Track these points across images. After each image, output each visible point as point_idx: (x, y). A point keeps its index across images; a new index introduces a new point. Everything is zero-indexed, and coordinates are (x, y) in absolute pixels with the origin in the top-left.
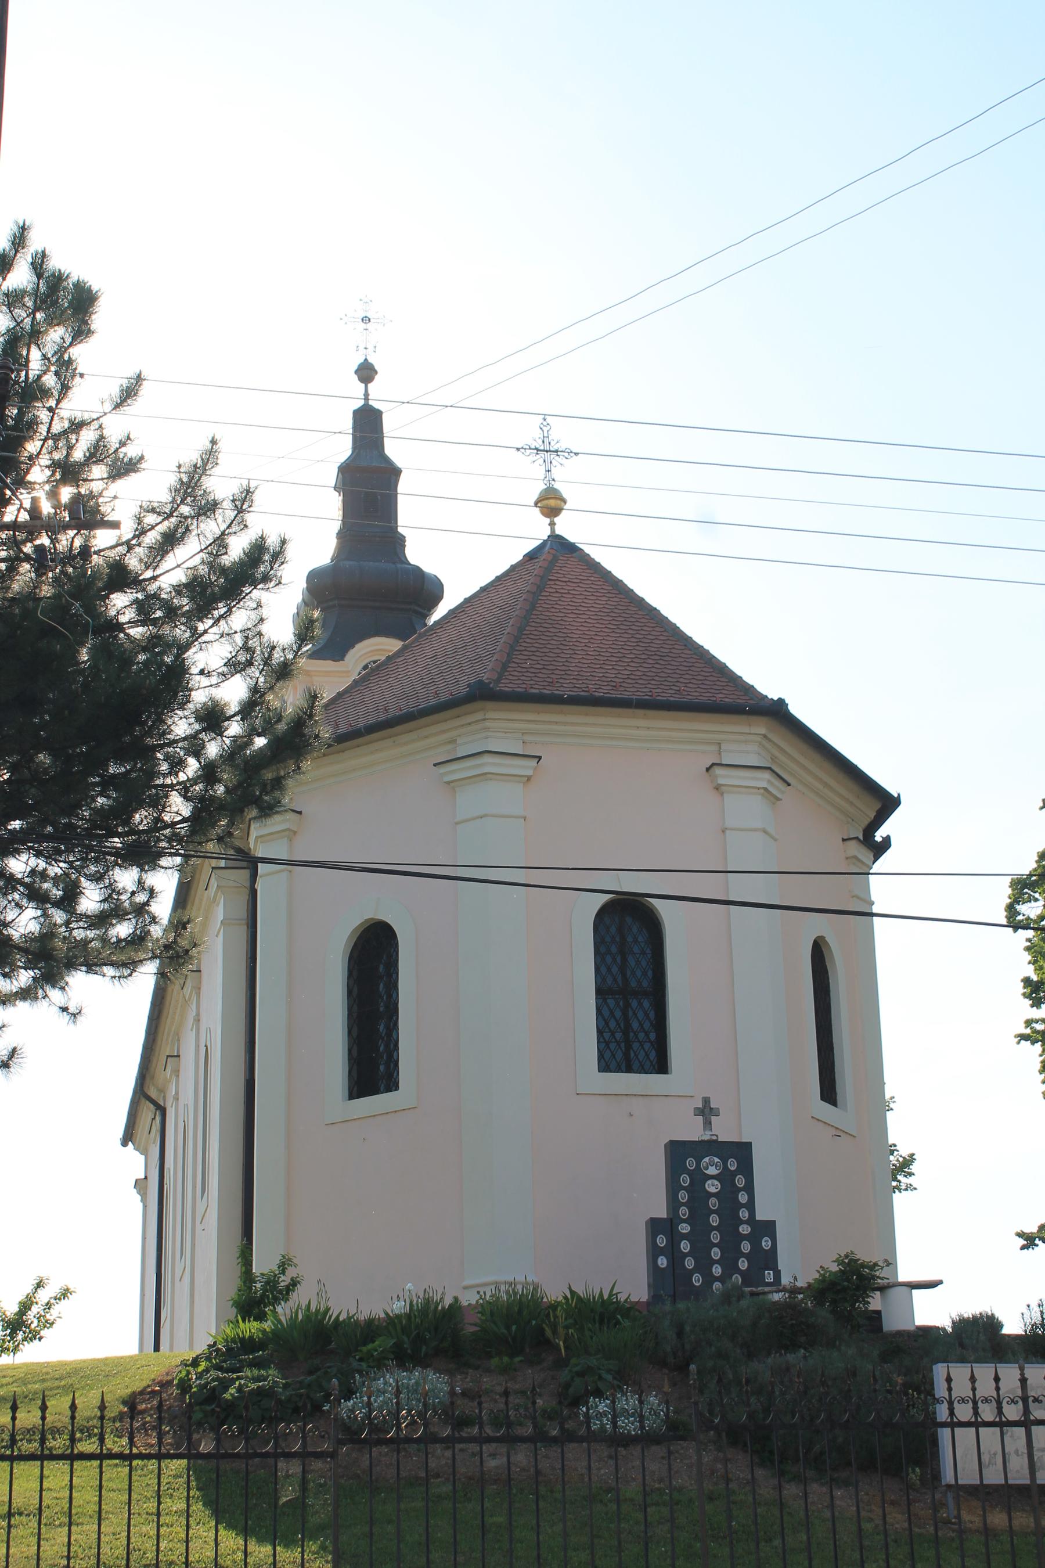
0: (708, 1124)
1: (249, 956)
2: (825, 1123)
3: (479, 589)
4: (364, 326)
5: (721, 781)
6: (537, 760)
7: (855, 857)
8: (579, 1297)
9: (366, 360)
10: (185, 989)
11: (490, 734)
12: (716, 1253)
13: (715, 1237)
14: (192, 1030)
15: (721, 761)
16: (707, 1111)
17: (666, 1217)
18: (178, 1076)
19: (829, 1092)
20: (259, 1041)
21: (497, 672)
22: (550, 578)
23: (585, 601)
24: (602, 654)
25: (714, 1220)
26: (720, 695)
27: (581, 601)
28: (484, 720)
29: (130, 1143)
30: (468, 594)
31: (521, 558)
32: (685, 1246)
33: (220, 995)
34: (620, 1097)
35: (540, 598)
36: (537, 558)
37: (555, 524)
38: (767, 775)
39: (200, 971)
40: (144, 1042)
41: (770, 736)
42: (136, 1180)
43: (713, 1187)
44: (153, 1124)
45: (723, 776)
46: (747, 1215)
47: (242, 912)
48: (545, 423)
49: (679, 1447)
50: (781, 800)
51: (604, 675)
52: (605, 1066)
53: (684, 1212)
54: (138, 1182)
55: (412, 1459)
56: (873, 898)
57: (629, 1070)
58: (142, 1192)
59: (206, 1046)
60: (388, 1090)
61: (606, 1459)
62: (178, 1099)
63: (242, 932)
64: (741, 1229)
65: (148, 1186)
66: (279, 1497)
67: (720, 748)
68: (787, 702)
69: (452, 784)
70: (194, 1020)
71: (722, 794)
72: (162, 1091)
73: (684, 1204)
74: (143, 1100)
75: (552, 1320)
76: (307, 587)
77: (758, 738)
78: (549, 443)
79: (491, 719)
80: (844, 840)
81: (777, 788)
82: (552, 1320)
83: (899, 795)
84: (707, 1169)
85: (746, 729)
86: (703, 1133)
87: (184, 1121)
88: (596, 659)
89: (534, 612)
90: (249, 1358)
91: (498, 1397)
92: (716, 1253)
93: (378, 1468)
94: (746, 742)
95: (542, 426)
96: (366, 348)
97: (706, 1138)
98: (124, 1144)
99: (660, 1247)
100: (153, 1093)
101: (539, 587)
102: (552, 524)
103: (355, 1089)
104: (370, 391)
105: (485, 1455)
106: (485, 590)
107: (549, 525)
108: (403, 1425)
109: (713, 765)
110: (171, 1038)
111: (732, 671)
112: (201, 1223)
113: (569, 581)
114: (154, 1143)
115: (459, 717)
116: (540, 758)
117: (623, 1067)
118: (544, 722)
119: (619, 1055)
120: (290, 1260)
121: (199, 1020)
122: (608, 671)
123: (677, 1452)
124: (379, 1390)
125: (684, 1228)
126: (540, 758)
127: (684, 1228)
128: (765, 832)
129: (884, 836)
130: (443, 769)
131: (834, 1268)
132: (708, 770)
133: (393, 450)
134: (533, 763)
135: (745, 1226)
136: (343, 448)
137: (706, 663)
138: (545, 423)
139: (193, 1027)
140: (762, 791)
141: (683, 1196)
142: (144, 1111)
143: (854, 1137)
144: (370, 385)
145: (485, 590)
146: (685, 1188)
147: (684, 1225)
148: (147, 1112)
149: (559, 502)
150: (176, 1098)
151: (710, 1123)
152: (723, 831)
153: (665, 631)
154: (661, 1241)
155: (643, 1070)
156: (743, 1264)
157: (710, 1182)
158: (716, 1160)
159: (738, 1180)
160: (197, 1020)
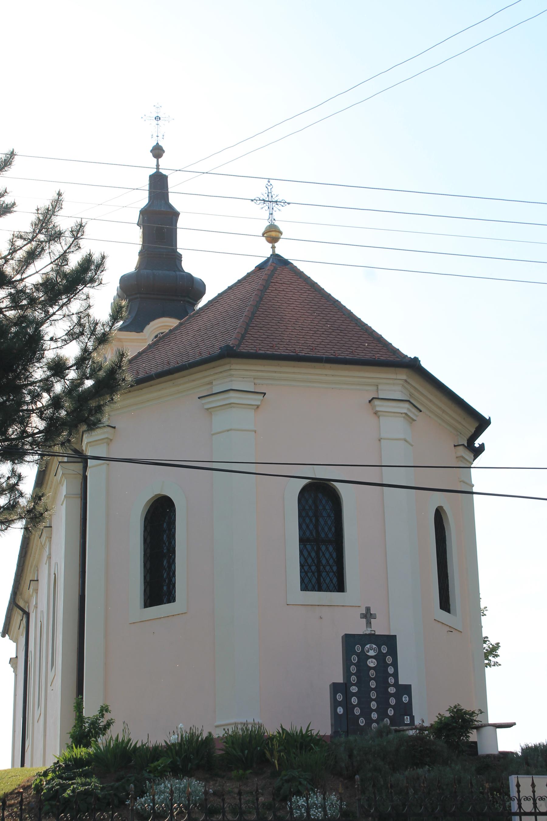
0: (369, 624)
5: (378, 409)
7: (462, 457)
8: (287, 732)
9: (157, 144)
12: (374, 705)
13: (373, 695)
15: (378, 395)
16: (368, 616)
18: (37, 593)
21: (238, 340)
22: (272, 281)
23: (293, 295)
25: (373, 684)
28: (230, 370)
29: (7, 635)
31: (254, 268)
32: (354, 700)
35: (265, 293)
36: (264, 268)
38: (407, 405)
39: (51, 527)
41: (409, 380)
42: (11, 659)
43: (372, 663)
46: (393, 681)
47: (78, 489)
48: (269, 184)
52: (305, 586)
53: (354, 679)
56: (473, 483)
57: (320, 589)
58: (14, 666)
59: (55, 574)
60: (169, 602)
62: (37, 607)
63: (78, 503)
64: (389, 690)
68: (419, 359)
71: (379, 417)
72: (27, 602)
75: (270, 747)
76: (120, 286)
78: (272, 197)
80: (455, 446)
82: (270, 747)
83: (490, 418)
84: (368, 652)
85: (394, 376)
86: (366, 629)
87: (41, 621)
90: (79, 771)
92: (374, 705)
95: (267, 186)
96: (157, 136)
97: (368, 632)
100: (21, 604)
101: (264, 286)
102: (273, 248)
103: (148, 601)
104: (160, 164)
106: (231, 288)
107: (271, 248)
108: (175, 814)
109: (373, 398)
115: (214, 368)
116: (265, 394)
117: (316, 588)
119: (314, 580)
121: (50, 558)
124: (161, 791)
126: (265, 394)
127: (354, 689)
128: (406, 440)
129: (481, 443)
131: (448, 714)
132: (370, 402)
133: (174, 200)
134: (261, 397)
135: (392, 688)
137: (369, 335)
138: (269, 184)
140: (404, 415)
141: (353, 669)
143: (461, 632)
144: (160, 160)
146: (354, 664)
147: (354, 687)
148: (18, 616)
149: (278, 233)
151: (370, 623)
152: (379, 440)
153: (344, 315)
154: (340, 697)
156: (391, 712)
157: (370, 660)
158: (374, 646)
159: (388, 659)
160: (49, 558)
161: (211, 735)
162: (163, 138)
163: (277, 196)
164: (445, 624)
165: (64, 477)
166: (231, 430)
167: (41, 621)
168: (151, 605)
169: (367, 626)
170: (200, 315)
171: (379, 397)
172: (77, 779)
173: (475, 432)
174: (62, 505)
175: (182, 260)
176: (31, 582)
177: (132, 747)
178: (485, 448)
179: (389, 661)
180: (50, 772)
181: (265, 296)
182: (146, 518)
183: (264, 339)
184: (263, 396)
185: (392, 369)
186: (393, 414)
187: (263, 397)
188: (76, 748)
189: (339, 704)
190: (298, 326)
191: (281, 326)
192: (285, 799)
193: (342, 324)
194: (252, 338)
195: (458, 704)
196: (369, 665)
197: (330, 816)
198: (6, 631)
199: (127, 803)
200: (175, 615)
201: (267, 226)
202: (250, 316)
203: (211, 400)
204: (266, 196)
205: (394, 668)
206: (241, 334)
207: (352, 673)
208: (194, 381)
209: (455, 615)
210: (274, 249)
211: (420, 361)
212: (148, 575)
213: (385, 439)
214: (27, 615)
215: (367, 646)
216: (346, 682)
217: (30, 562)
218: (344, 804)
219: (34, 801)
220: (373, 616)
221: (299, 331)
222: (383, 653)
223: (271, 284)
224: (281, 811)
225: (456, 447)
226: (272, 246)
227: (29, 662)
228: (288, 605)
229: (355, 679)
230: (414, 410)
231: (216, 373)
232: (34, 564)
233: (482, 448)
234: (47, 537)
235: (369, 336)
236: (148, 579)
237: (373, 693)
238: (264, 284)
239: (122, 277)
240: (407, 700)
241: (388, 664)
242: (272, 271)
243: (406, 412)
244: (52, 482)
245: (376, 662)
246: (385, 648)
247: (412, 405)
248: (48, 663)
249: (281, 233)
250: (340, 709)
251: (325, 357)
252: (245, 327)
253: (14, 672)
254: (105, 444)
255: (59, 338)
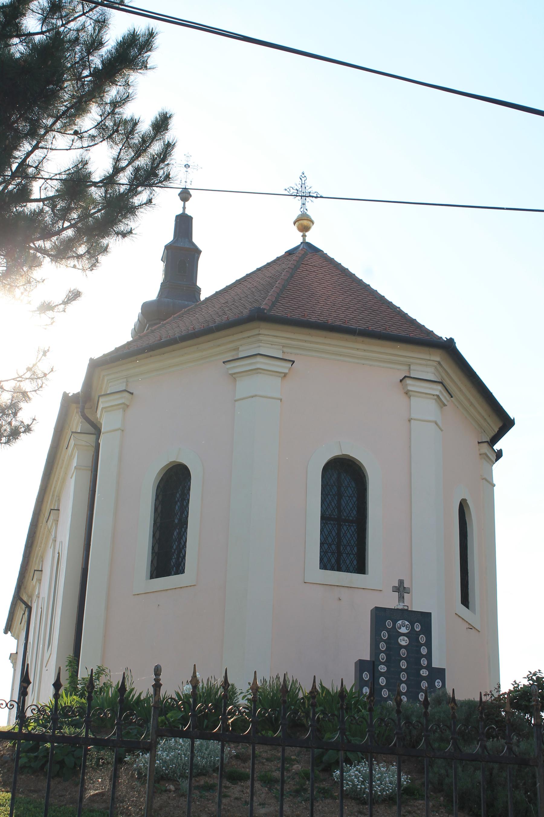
0: (401, 598)
1: (91, 489)
2: (463, 619)
3: (256, 269)
4: (186, 169)
5: (410, 388)
6: (292, 363)
7: (486, 454)
8: (328, 691)
10: (48, 522)
11: (261, 344)
13: (404, 676)
14: (51, 548)
15: (410, 374)
16: (401, 589)
17: (369, 660)
18: (40, 583)
19: (465, 601)
20: (92, 553)
21: (269, 306)
22: (303, 263)
23: (324, 277)
24: (335, 305)
25: (403, 665)
26: (412, 335)
27: (322, 277)
28: (259, 334)
29: (9, 632)
30: (249, 272)
31: (284, 253)
32: (382, 681)
33: (70, 519)
34: (333, 587)
35: (296, 272)
36: (294, 254)
37: (306, 236)
38: (439, 387)
39: (59, 510)
40: (21, 563)
41: (442, 363)
42: (11, 654)
43: (403, 641)
44: (24, 618)
45: (412, 385)
46: (426, 663)
47: (89, 462)
48: (303, 176)
49: (416, 808)
50: (447, 406)
51: (338, 316)
52: (324, 565)
54: (12, 655)
55: (195, 803)
56: (494, 482)
57: (339, 569)
58: (14, 661)
59: (59, 553)
60: (177, 573)
61: (356, 814)
62: (39, 597)
63: (88, 475)
64: (421, 672)
65: (18, 659)
66: (86, 789)
67: (410, 368)
68: (455, 341)
69: (234, 376)
70: (53, 540)
71: (409, 397)
72: (30, 597)
73: (383, 652)
74: (19, 601)
75: (307, 707)
76: (141, 313)
77: (435, 364)
78: (305, 188)
79: (262, 334)
80: (479, 443)
81: (444, 397)
82: (307, 707)
83: (514, 419)
84: (400, 628)
85: (427, 357)
86: (398, 604)
87: (41, 608)
88: (332, 307)
89: (292, 279)
90: (68, 720)
91: (264, 761)
93: (167, 809)
94: (426, 365)
95: (301, 177)
96: (186, 182)
97: (400, 607)
98: (6, 632)
99: (364, 680)
100: (25, 598)
101: (295, 266)
102: (304, 236)
103: (155, 572)
104: (186, 206)
105: (255, 804)
106: (260, 270)
107: (302, 236)
108: (230, 721)
109: (405, 377)
110: (38, 559)
111: (420, 324)
112: (46, 667)
113: (314, 266)
114: (23, 630)
115: (242, 332)
116: (293, 362)
117: (336, 568)
118: (298, 339)
119: (333, 561)
120: (103, 670)
121: (56, 541)
122: (340, 314)
123: (414, 812)
124: (170, 748)
125: (383, 668)
126: (293, 362)
127: (383, 668)
128: (436, 423)
130: (229, 365)
131: (526, 682)
132: (401, 381)
133: (197, 238)
134: (289, 365)
135: (424, 670)
136: (169, 237)
137: (402, 317)
138: (303, 176)
139: (51, 546)
140: (436, 397)
141: (383, 646)
142: (19, 610)
143: (479, 631)
144: (186, 203)
145: (260, 270)
146: (384, 641)
147: (383, 666)
148: (21, 609)
149: (309, 222)
150: (38, 597)
151: (403, 597)
152: (409, 421)
153: (375, 298)
154: (366, 676)
155: (348, 571)
157: (401, 638)
158: (407, 623)
159: (421, 638)
160: (55, 540)
161: (233, 689)
162: (191, 184)
163: (310, 188)
164: (465, 621)
165: (75, 448)
166: (256, 396)
167: (41, 608)
168: (157, 577)
169: (399, 600)
170: (227, 292)
171: (411, 376)
172: (64, 728)
173: (498, 431)
174: (71, 478)
175: (200, 294)
176: (35, 572)
177: (134, 699)
178: (503, 454)
179: (422, 640)
180: (32, 721)
181: (296, 274)
182: (158, 486)
183: (295, 309)
184: (291, 364)
185: (426, 349)
186: (424, 395)
187: (292, 365)
188: (67, 696)
189: (366, 684)
190: (330, 302)
191: (312, 300)
192: (328, 769)
193: (374, 305)
194: (283, 307)
195: (539, 671)
196: (400, 643)
197: (391, 791)
198: (8, 628)
199: (126, 759)
200: (183, 587)
201: (299, 215)
202: (281, 288)
203: (235, 365)
204: (300, 186)
205: (427, 649)
206: (272, 301)
207: (381, 650)
208: (219, 346)
209: (474, 611)
210: (304, 237)
211: (455, 343)
212: (157, 546)
213: (415, 420)
214: (29, 608)
215: (399, 622)
216: (374, 660)
217: (36, 552)
218: (408, 778)
219: (8, 754)
220: (407, 591)
221: (330, 306)
222: (416, 631)
223: (301, 265)
224: (324, 783)
225: (479, 444)
226: (303, 234)
227: (27, 653)
228: (305, 583)
229: (384, 656)
230: (446, 394)
231: (244, 338)
232: (39, 555)
233: (499, 455)
234: (54, 520)
235: (401, 318)
236: (156, 550)
237: (403, 674)
238: (295, 264)
239: (144, 303)
240: (440, 685)
241: (422, 643)
242: (303, 255)
243: (438, 394)
244: (63, 461)
245: (408, 640)
246: (419, 626)
247: (444, 388)
248: (45, 645)
249: (313, 222)
250: (366, 689)
251: (359, 329)
252: (276, 296)
253: (13, 667)
254: (121, 410)
255: (86, 132)
